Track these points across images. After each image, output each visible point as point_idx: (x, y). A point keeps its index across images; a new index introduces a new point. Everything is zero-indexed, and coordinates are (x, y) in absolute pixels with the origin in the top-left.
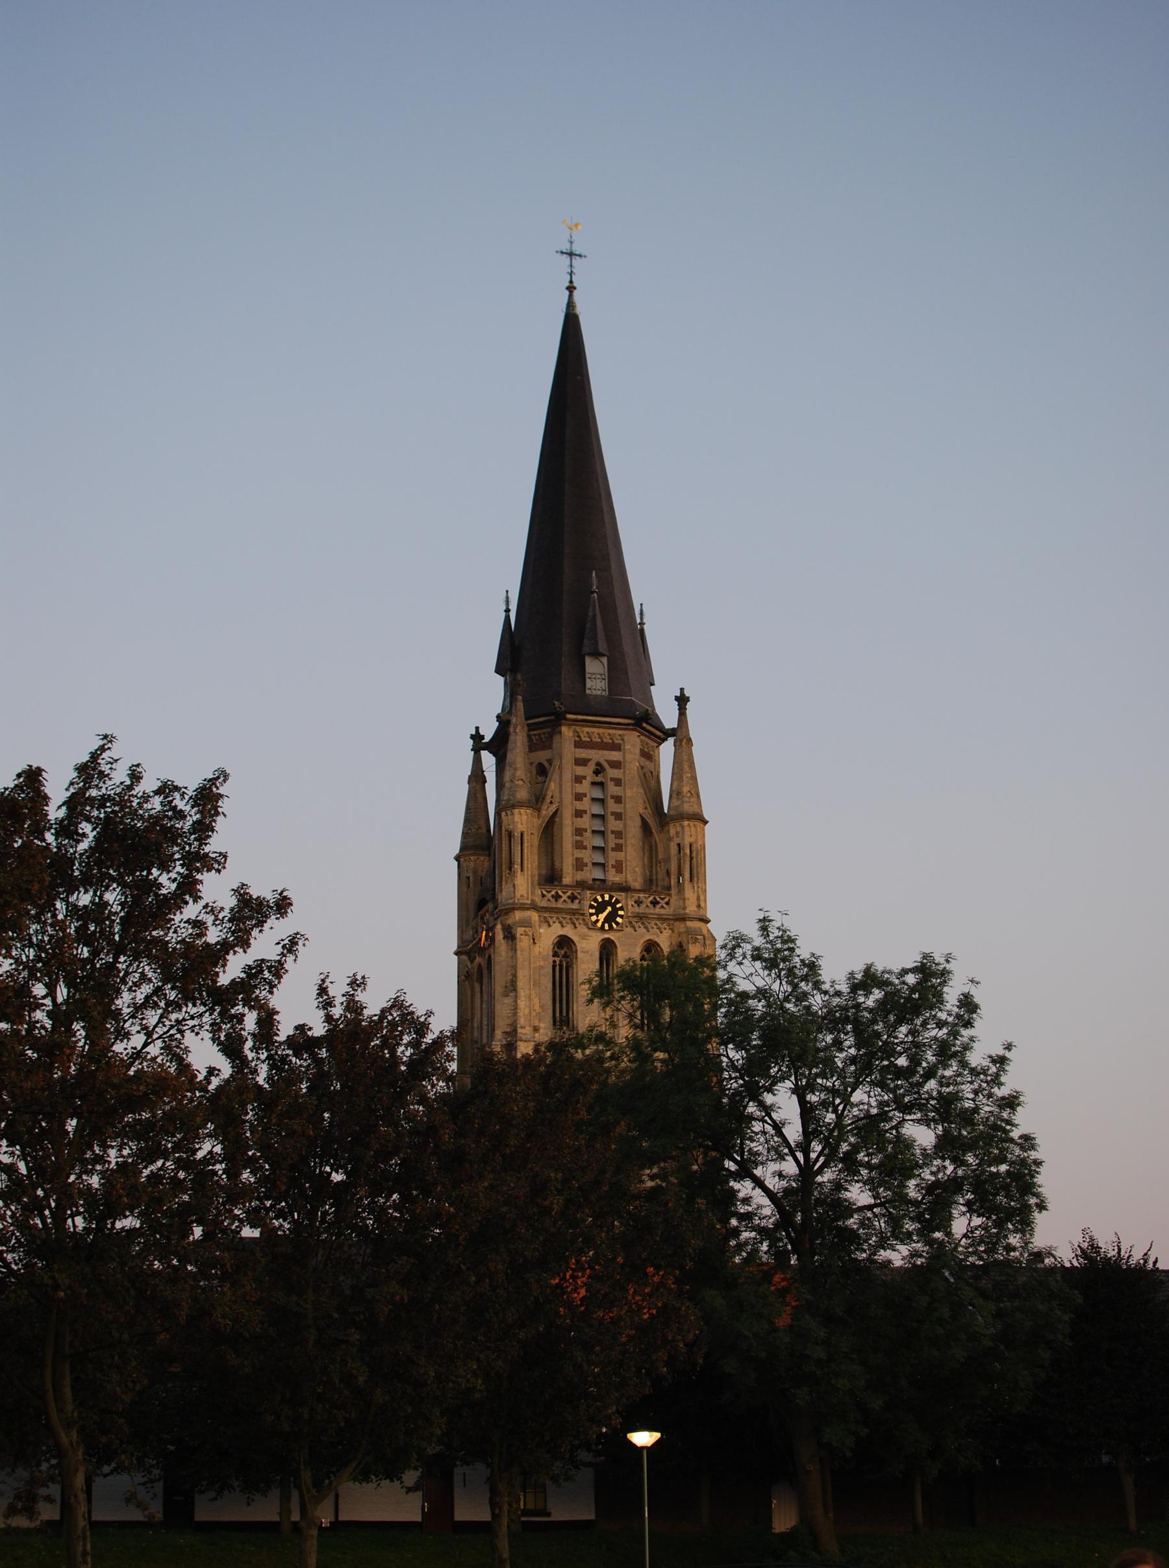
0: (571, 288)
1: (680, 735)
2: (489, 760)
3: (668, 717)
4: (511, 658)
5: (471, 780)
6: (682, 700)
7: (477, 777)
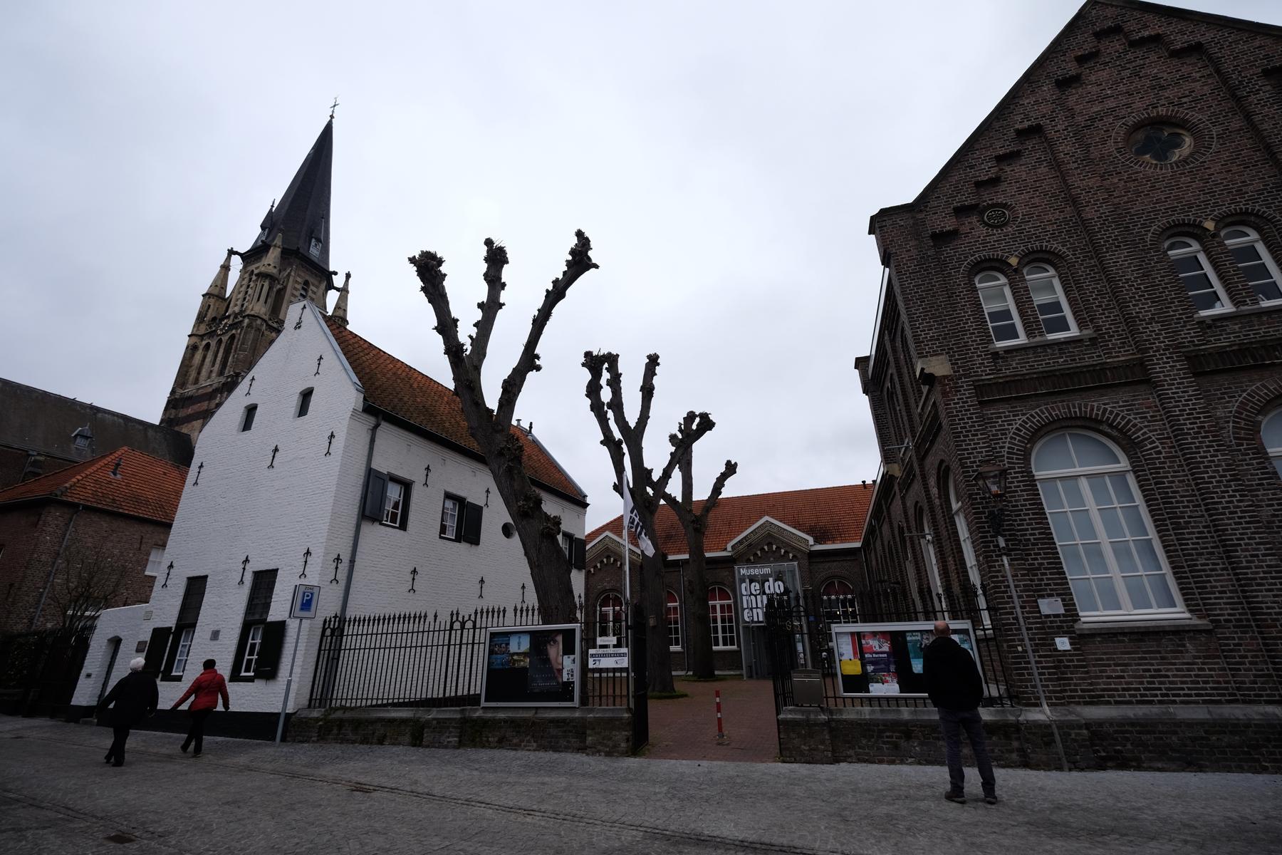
0: (332, 117)
1: (344, 291)
2: (237, 263)
3: (338, 281)
4: (271, 223)
5: (222, 267)
6: (348, 276)
7: (226, 268)
